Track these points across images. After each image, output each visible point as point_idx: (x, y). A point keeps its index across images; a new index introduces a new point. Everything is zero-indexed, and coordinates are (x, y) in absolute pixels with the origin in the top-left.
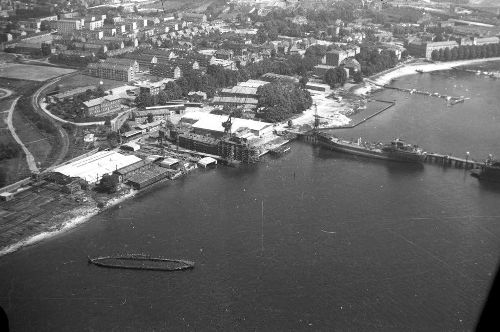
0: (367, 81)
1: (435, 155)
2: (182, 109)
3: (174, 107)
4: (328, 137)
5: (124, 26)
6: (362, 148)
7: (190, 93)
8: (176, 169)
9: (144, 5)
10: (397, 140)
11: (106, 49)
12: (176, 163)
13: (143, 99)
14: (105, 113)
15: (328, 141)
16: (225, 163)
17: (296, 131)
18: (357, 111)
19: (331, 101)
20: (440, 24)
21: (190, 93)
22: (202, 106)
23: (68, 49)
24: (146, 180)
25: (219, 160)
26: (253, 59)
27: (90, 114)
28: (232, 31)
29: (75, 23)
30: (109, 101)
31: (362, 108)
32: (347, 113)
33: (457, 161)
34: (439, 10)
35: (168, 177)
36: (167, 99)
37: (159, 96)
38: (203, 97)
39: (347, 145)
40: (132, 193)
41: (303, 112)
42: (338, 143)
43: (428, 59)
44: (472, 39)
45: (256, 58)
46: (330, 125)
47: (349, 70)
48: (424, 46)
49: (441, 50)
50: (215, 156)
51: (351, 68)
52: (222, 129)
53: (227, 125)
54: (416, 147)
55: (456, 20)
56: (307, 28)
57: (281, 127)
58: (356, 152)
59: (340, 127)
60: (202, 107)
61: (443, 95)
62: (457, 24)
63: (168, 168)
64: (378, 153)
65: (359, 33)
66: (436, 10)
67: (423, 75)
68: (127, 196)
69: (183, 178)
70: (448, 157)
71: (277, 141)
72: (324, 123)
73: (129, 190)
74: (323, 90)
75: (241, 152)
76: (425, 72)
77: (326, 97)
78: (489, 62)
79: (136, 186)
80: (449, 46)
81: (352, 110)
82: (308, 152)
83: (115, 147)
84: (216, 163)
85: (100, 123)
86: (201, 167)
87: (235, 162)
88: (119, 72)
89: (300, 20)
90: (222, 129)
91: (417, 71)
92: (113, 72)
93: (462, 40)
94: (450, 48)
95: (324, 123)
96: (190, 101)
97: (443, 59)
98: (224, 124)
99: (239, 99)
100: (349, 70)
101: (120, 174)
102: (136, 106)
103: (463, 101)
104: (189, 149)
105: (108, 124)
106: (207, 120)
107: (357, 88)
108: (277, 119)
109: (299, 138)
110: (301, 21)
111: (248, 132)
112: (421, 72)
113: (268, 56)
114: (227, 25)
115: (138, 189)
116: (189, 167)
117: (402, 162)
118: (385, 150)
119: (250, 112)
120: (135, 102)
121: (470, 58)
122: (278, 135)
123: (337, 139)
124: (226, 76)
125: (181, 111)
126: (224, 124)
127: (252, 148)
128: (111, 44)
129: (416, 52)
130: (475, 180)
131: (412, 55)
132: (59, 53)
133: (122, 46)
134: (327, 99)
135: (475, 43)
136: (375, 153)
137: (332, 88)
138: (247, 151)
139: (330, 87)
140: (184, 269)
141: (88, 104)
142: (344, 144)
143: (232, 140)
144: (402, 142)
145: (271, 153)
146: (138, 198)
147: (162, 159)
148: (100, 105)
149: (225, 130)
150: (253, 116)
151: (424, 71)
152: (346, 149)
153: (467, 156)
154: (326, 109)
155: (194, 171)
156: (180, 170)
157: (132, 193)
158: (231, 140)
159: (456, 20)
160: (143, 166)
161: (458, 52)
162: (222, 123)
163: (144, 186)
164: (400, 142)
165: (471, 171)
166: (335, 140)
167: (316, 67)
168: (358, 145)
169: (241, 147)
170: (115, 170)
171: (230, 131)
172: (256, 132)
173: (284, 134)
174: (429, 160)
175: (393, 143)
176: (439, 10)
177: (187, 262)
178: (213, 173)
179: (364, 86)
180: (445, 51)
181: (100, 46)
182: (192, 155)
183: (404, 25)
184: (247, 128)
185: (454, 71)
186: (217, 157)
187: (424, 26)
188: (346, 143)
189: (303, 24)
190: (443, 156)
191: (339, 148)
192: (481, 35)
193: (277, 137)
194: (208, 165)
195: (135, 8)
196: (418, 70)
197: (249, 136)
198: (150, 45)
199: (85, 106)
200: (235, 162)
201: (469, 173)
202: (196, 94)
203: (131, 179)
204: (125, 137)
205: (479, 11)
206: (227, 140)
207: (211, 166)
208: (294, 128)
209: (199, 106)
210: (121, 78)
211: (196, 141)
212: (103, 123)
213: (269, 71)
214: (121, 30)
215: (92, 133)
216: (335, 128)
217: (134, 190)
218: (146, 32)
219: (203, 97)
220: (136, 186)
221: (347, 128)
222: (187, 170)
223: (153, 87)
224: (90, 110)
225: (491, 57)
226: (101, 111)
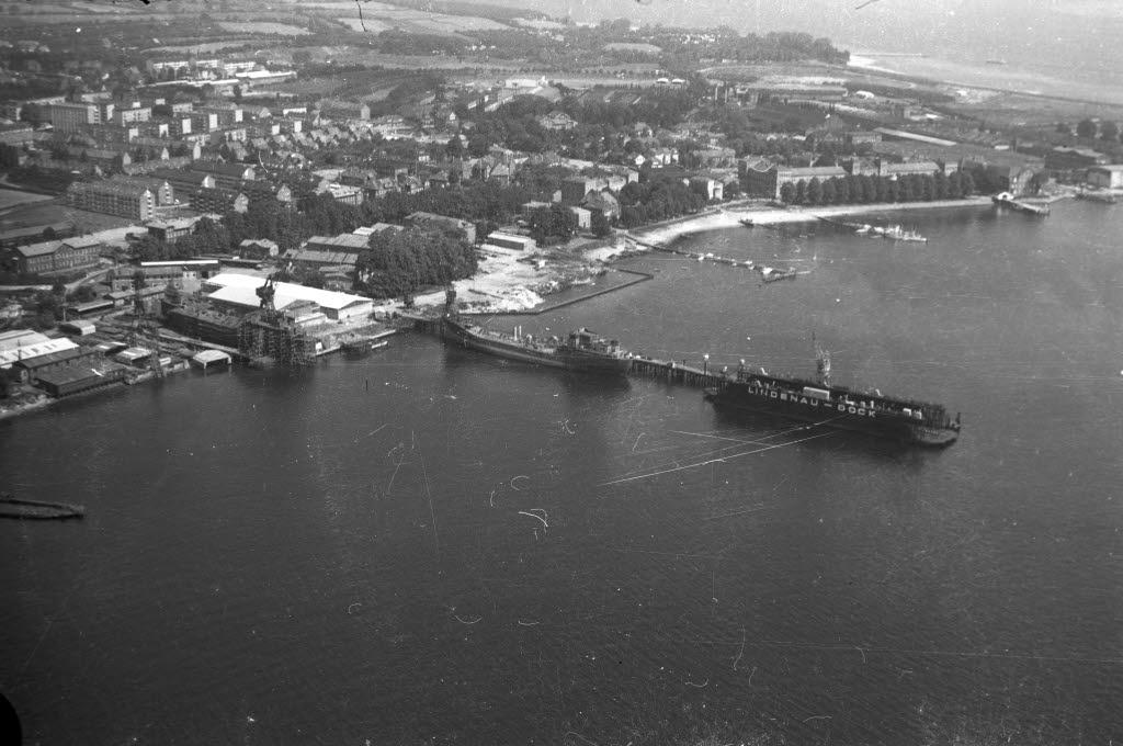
0: (621, 236)
1: (655, 361)
2: (214, 269)
3: (198, 265)
4: (462, 324)
5: (189, 120)
6: (522, 345)
7: (246, 243)
8: (141, 367)
9: (262, 85)
10: (582, 330)
11: (127, 160)
12: (147, 357)
13: (152, 245)
14: (63, 271)
15: (462, 332)
16: (247, 360)
17: (418, 315)
18: (566, 287)
19: (528, 269)
20: (849, 139)
21: (246, 243)
22: (259, 266)
23: (53, 158)
24: (72, 380)
25: (234, 356)
26: (408, 188)
27: (31, 270)
28: (380, 128)
29: (86, 110)
30: (75, 249)
31: (579, 282)
32: (542, 290)
33: (691, 373)
34: (854, 109)
35: (123, 379)
36: (195, 251)
37: (178, 244)
38: (268, 250)
39: (495, 339)
40: (42, 401)
41: (453, 282)
42: (481, 336)
43: (778, 201)
44: (877, 164)
45: (413, 186)
46: (493, 308)
47: (589, 213)
48: (773, 173)
49: (801, 183)
50: (230, 349)
51: (596, 210)
52: (256, 301)
53: (266, 294)
54: (614, 343)
55: (888, 132)
56: (566, 136)
57: (392, 306)
58: (509, 352)
59: (513, 313)
60: (259, 269)
61: (184, 161)
62: (886, 138)
63: (129, 365)
64: (548, 356)
65: (666, 149)
66: (863, 110)
67: (754, 230)
68: (28, 406)
69: (157, 384)
70: (674, 366)
71: (370, 330)
72: (483, 304)
73: (37, 396)
74: (520, 247)
75: (278, 341)
76: (758, 225)
77: (518, 261)
78: (904, 210)
79: (51, 390)
80: (805, 178)
81: (554, 284)
82: (433, 357)
83: (49, 328)
84: (230, 360)
85: (43, 288)
86: (197, 366)
87: (266, 360)
88: (123, 200)
89: (557, 121)
90: (256, 301)
91: (742, 222)
92: (113, 201)
93: (855, 165)
94: (821, 179)
95: (483, 304)
96: (242, 257)
97: (808, 201)
98: (260, 292)
99: (333, 254)
100: (589, 213)
101: (24, 367)
102: (129, 261)
103: (793, 278)
104: (190, 336)
105: (58, 289)
106: (238, 286)
107: (595, 247)
108: (387, 291)
109: (420, 327)
110: (557, 122)
111: (314, 312)
112: (748, 225)
113: (444, 182)
114: (408, 128)
115: (55, 397)
116: (171, 365)
117: (591, 374)
118: (561, 350)
119: (341, 279)
120: (128, 253)
121: (866, 200)
122: (376, 320)
123: (498, 335)
124: (330, 214)
125: (210, 273)
126: (260, 292)
127: (299, 336)
128: (139, 151)
129: (755, 187)
130: (709, 407)
131: (748, 191)
132: (33, 163)
133: (165, 155)
134: (518, 264)
135: (883, 172)
136: (541, 354)
137: (540, 244)
138: (288, 342)
139: (534, 242)
140: (63, 518)
141: (27, 250)
142: (489, 338)
143: (265, 321)
144: (589, 334)
145: (350, 352)
146: (51, 409)
147: (120, 349)
148: (52, 254)
149: (262, 303)
150: (348, 286)
151: (754, 222)
152: (492, 348)
153: (703, 361)
154: (505, 281)
155: (183, 374)
156: (151, 369)
157: (42, 401)
158: (263, 320)
159: (888, 132)
160: (78, 358)
161: (837, 188)
162: (257, 290)
163: (66, 391)
164: (586, 334)
165: (706, 393)
166: (475, 331)
167: (528, 205)
168: (514, 340)
169: (277, 332)
170: (17, 359)
171: (272, 304)
172: (331, 312)
173: (387, 320)
174: (641, 370)
175: (573, 337)
176: (854, 109)
177: (72, 507)
178: (226, 381)
179: (612, 244)
180: (810, 184)
181: (115, 154)
182: (189, 346)
183: (772, 137)
184: (313, 304)
185: (812, 227)
186: (234, 351)
187: (813, 141)
188: (495, 336)
189: (563, 129)
190: (665, 364)
191: (481, 345)
192: (906, 159)
193: (375, 323)
194: (208, 363)
195: (236, 89)
196: (744, 219)
197: (306, 320)
198: (220, 157)
199: (21, 255)
200: (266, 360)
201: (699, 395)
202: (254, 244)
203: (46, 378)
204: (76, 311)
205: (961, 116)
206: (257, 320)
207: (217, 366)
208: (417, 309)
209: (253, 266)
210: (126, 210)
211: (203, 322)
212: (50, 288)
213: (420, 210)
214: (181, 127)
215: (20, 302)
216: (503, 313)
217: (48, 397)
218: (227, 134)
219: (268, 250)
220: (51, 390)
221: (530, 314)
222: (166, 370)
223: (172, 227)
224: (30, 261)
225: (912, 200)
226: (54, 265)
